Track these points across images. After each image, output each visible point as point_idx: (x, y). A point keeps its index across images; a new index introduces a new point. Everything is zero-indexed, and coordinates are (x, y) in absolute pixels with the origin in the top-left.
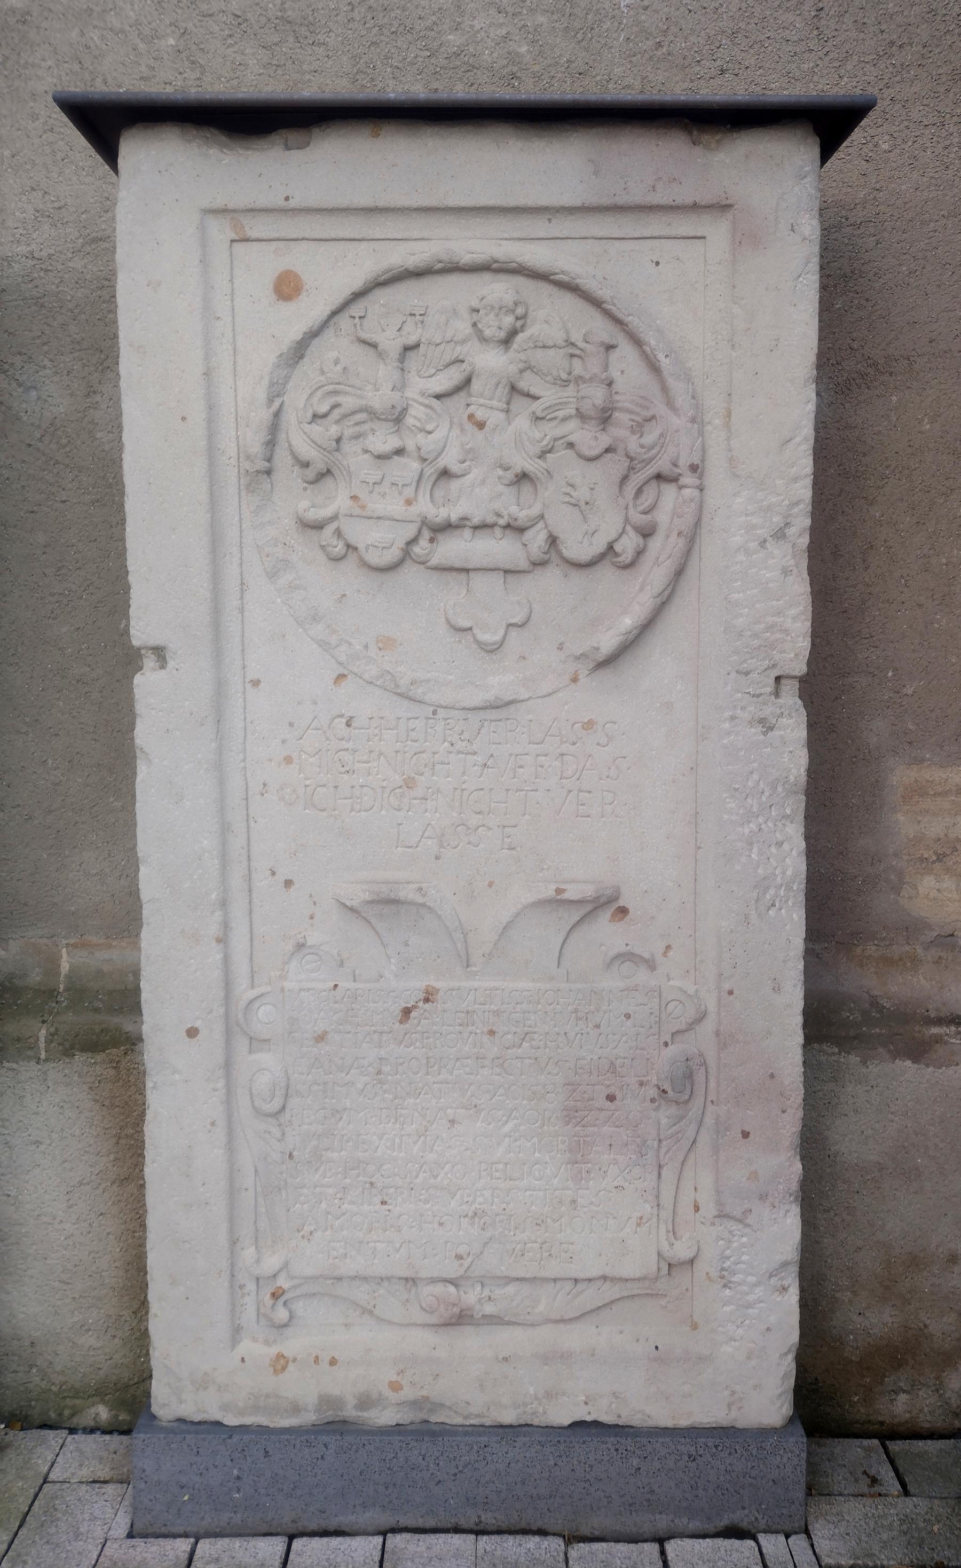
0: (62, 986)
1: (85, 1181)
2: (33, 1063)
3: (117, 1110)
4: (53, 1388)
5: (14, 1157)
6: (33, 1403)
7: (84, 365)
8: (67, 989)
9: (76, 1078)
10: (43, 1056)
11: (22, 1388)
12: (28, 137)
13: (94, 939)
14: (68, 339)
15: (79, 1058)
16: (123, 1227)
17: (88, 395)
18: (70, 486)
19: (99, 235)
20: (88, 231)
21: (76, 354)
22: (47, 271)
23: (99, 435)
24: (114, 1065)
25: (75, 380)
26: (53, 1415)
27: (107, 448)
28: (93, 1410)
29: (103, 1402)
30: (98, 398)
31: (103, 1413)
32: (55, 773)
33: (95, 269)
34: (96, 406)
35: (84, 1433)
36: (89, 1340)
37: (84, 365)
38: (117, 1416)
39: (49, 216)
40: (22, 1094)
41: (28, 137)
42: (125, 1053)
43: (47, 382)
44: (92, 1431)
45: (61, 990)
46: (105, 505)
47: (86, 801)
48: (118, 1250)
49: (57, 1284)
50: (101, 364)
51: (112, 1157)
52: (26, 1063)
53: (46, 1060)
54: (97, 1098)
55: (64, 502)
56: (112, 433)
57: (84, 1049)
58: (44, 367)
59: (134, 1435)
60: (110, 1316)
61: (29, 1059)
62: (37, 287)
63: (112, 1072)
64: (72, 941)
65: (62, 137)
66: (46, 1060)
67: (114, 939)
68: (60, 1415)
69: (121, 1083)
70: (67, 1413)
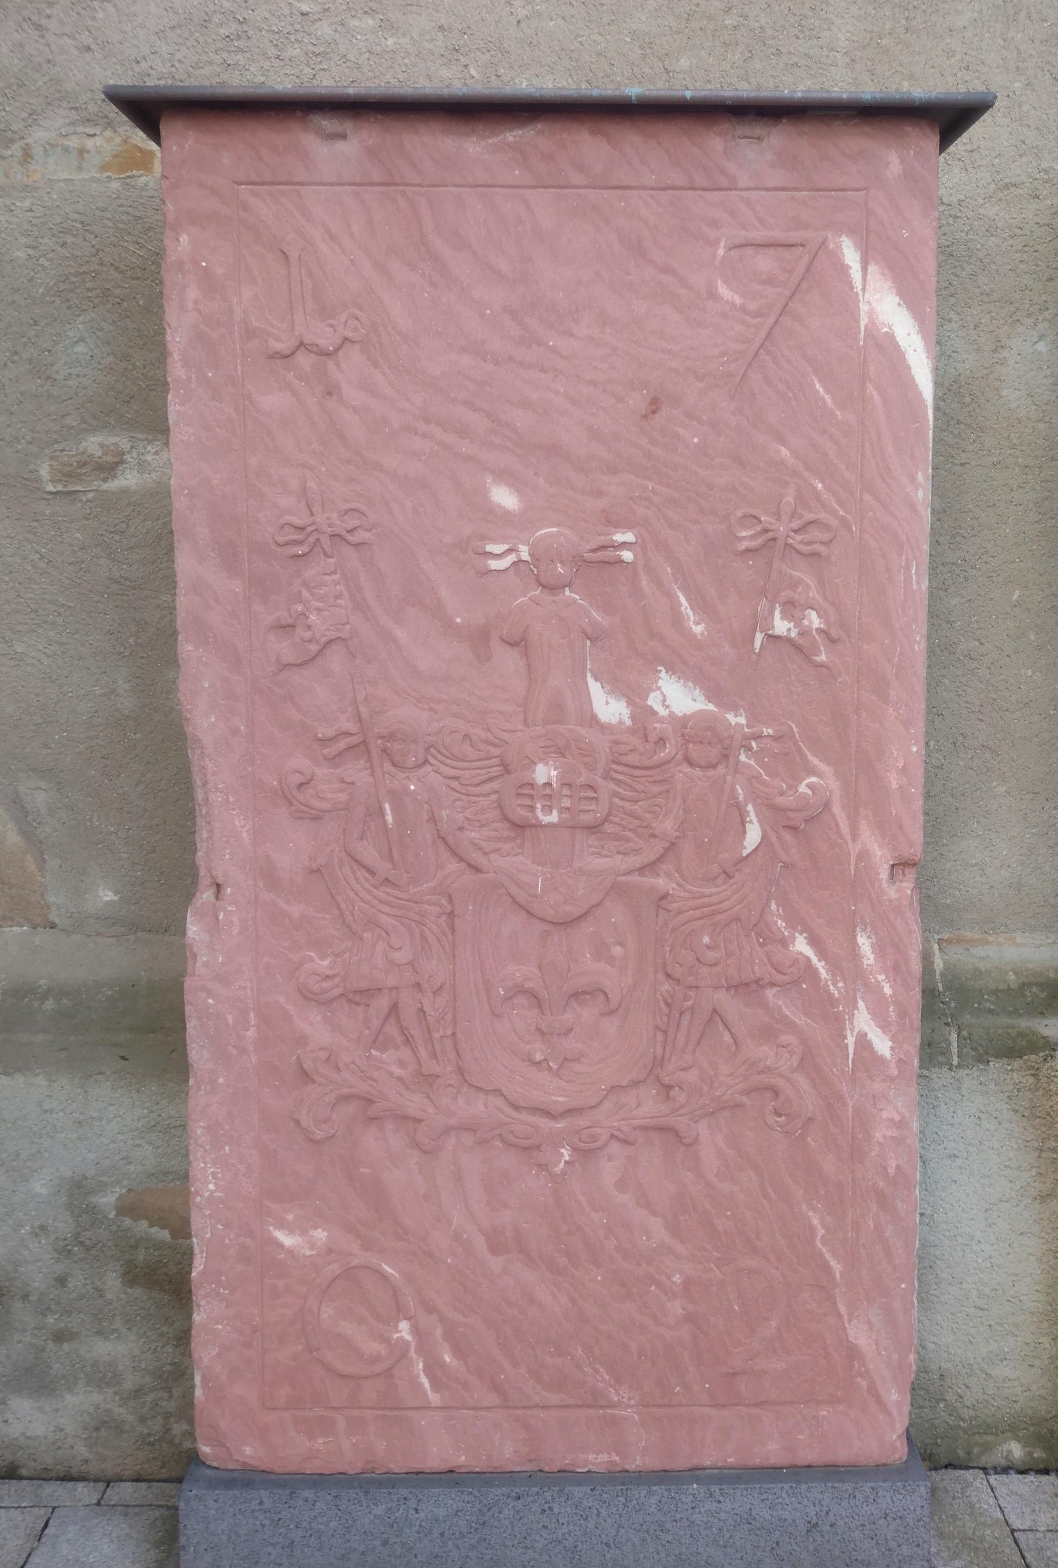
0: (940, 985)
1: (1005, 1198)
2: (945, 1069)
3: (1038, 1120)
4: (961, 1423)
5: (929, 1172)
6: (939, 1441)
7: (993, 318)
8: (947, 988)
9: (992, 1086)
10: (955, 1061)
11: (926, 1425)
12: (942, 75)
13: (968, 934)
14: (977, 291)
15: (995, 1064)
16: (1044, 1247)
17: (995, 351)
18: (970, 448)
19: (1014, 180)
20: (1001, 176)
21: (984, 307)
22: (955, 217)
23: (1004, 393)
24: (1033, 1072)
25: (982, 334)
26: (961, 1453)
27: (1013, 406)
28: (1005, 1447)
29: (1018, 1439)
30: (1005, 353)
31: (1016, 1450)
32: (937, 755)
33: (1007, 217)
34: (1003, 362)
35: (996, 1473)
36: (1002, 1371)
37: (993, 318)
38: (1031, 1454)
39: (959, 159)
40: (935, 1103)
41: (942, 75)
42: (1045, 1060)
43: (953, 336)
44: (1005, 1470)
45: (941, 989)
46: (1007, 467)
47: (967, 786)
48: (1039, 1272)
49: (971, 1310)
50: (1011, 317)
51: (1034, 1172)
52: (937, 1070)
53: (959, 1066)
54: (1016, 1107)
55: (962, 465)
56: (1019, 390)
57: (999, 1055)
58: (950, 321)
59: (185, 1486)
60: (1027, 1344)
61: (941, 1065)
62: (945, 234)
63: (1031, 1080)
64: (946, 936)
65: (977, 75)
66: (959, 1066)
67: (990, 934)
68: (969, 1453)
69: (1040, 1092)
70: (976, 1450)
